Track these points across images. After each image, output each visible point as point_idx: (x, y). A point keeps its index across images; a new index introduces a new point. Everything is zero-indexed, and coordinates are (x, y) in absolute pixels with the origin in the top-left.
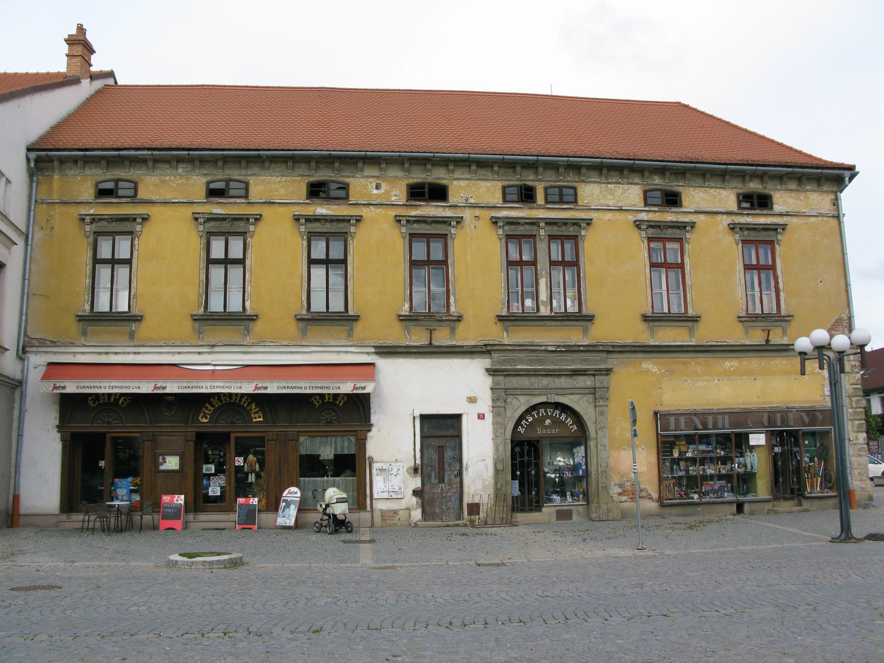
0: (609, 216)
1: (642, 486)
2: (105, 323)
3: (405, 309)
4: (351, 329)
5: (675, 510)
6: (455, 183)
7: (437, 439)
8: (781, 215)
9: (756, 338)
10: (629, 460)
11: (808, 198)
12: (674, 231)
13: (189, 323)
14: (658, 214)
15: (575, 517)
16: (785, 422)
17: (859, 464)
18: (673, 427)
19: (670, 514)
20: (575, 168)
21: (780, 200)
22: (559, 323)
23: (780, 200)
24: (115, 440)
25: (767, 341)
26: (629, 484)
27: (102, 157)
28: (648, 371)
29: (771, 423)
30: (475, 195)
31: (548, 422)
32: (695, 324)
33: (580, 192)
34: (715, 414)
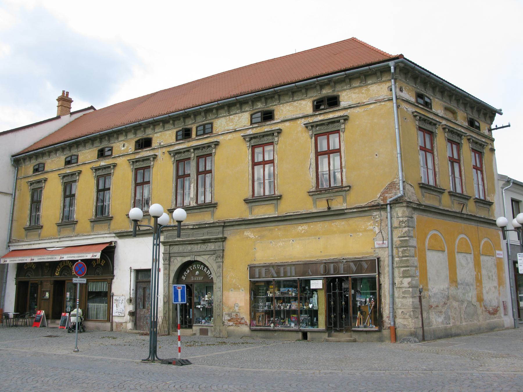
0: (230, 136)
1: (241, 316)
2: (32, 231)
3: (249, 195)
4: (110, 225)
5: (260, 334)
6: (155, 135)
7: (143, 283)
8: (345, 109)
9: (322, 206)
10: (234, 298)
11: (369, 90)
12: (268, 137)
13: (56, 227)
14: (259, 128)
15: (209, 334)
16: (336, 270)
17: (402, 305)
18: (257, 276)
19: (257, 336)
20: (208, 111)
21: (346, 97)
22: (198, 210)
23: (346, 97)
24: (80, 284)
25: (329, 208)
26: (234, 314)
27: (361, 73)
28: (248, 237)
29: (326, 271)
30: (165, 138)
31: (197, 273)
32: (215, 209)
33: (215, 125)
34: (283, 265)
